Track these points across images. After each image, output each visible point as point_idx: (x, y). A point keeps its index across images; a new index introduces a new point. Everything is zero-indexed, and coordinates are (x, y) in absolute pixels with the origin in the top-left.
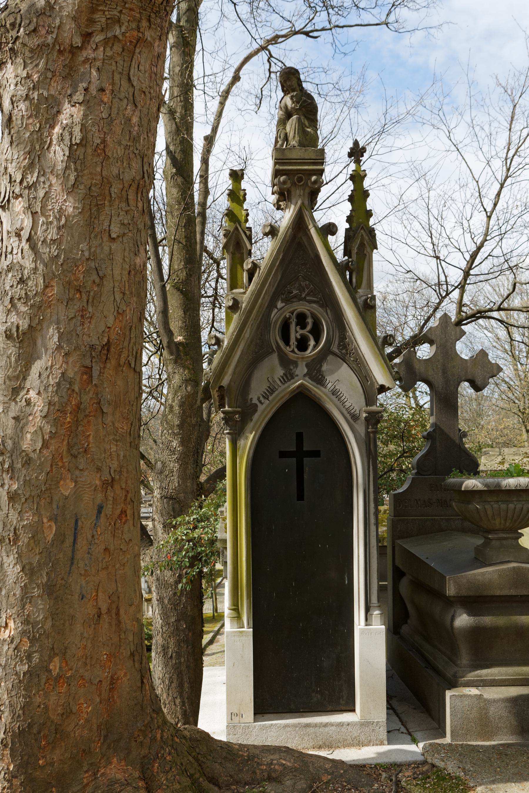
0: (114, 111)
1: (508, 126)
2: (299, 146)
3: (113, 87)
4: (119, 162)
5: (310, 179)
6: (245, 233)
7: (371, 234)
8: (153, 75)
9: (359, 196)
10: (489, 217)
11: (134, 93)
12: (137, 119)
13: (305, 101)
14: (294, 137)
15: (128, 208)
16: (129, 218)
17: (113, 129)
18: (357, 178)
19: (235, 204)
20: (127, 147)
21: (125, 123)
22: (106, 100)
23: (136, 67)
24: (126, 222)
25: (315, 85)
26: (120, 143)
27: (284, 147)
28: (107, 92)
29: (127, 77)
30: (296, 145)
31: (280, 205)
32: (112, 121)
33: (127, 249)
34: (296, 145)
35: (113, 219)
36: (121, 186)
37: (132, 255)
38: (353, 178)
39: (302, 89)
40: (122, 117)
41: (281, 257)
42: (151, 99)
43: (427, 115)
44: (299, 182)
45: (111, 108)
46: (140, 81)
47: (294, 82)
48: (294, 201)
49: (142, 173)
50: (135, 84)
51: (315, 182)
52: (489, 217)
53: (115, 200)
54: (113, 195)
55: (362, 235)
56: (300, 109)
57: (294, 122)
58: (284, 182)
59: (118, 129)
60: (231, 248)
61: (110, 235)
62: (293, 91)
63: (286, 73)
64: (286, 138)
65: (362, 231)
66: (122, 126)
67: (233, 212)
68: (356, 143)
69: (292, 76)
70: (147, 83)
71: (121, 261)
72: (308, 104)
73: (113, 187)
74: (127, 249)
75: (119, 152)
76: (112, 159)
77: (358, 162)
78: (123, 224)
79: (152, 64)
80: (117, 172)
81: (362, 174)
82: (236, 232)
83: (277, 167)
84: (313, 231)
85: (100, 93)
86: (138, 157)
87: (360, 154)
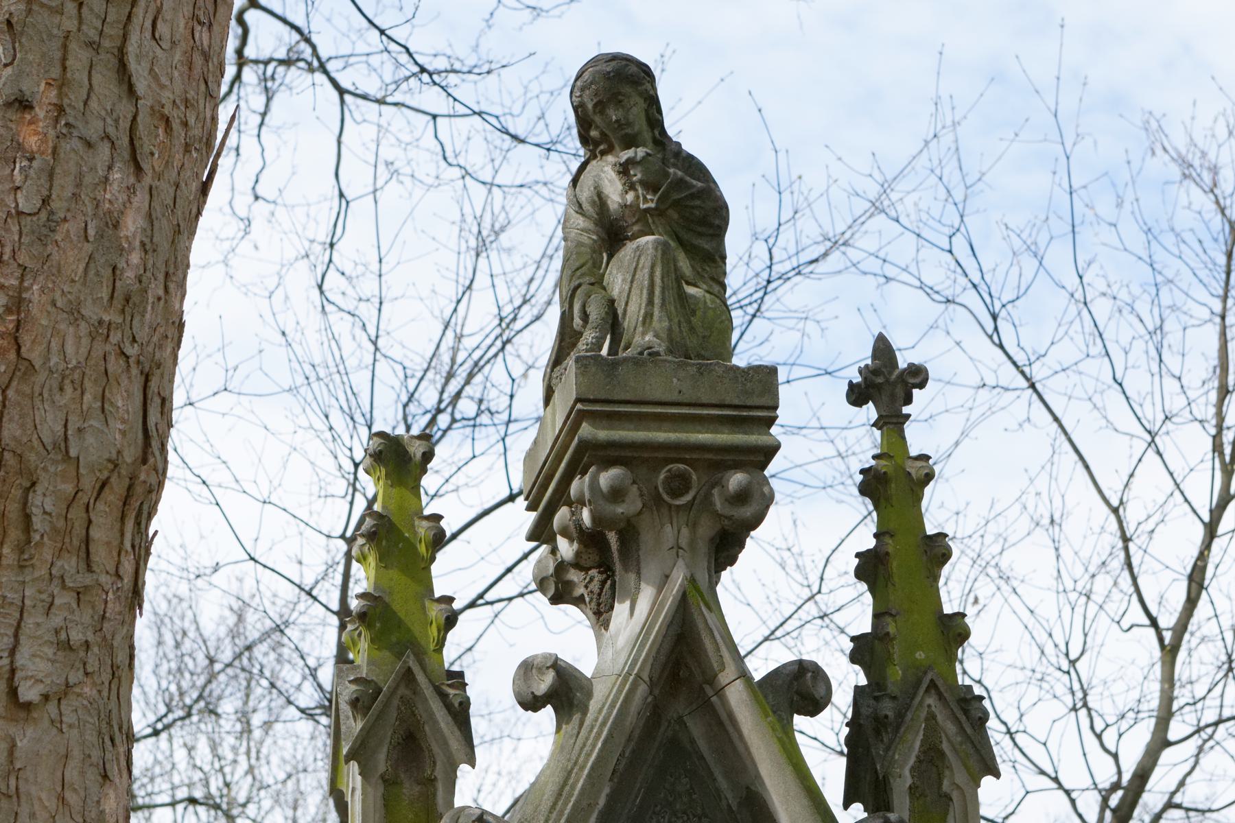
0: (64, 187)
1: (1217, 306)
2: (670, 351)
3: (60, 95)
4: (69, 389)
5: (719, 483)
6: (443, 696)
7: (966, 712)
8: (198, 60)
9: (903, 561)
10: (1170, 652)
11: (134, 118)
12: (141, 222)
13: (679, 184)
14: (648, 316)
15: (88, 580)
16: (86, 619)
17: (56, 257)
18: (894, 484)
19: (394, 574)
20: (101, 330)
21: (100, 235)
22: (32, 142)
23: (148, 24)
24: (76, 636)
25: (429, 118)
26: (74, 313)
27: (604, 352)
28: (40, 112)
29: (114, 62)
30: (660, 347)
31: (569, 585)
32: (52, 224)
33: (76, 753)
34: (660, 347)
35: (29, 622)
36: (69, 488)
37: (93, 776)
38: (874, 485)
39: (661, 140)
40: (89, 209)
41: (602, 802)
42: (187, 148)
43: (903, 249)
44: (676, 494)
45: (51, 176)
46: (156, 78)
47: (637, 111)
48: (651, 569)
49: (140, 435)
50: (141, 87)
51: (742, 497)
52: (1170, 652)
53: (40, 544)
54: (38, 522)
55: (931, 717)
56: (658, 212)
57: (646, 261)
58: (616, 494)
59: (72, 259)
60: (382, 756)
61: (13, 692)
62: (630, 142)
63: (607, 76)
64: (613, 323)
65: (931, 701)
66: (88, 248)
67: (387, 606)
68: (883, 349)
69: (627, 89)
70: (178, 86)
71: (52, 804)
72: (692, 196)
73: (39, 489)
74: (76, 753)
75: (70, 349)
76: (41, 377)
77: (892, 422)
78: (67, 646)
79: (194, 17)
80: (59, 428)
81: (914, 469)
82: (402, 691)
83: (586, 430)
84: (736, 696)
85: (11, 114)
86: (135, 371)
87: (900, 392)
